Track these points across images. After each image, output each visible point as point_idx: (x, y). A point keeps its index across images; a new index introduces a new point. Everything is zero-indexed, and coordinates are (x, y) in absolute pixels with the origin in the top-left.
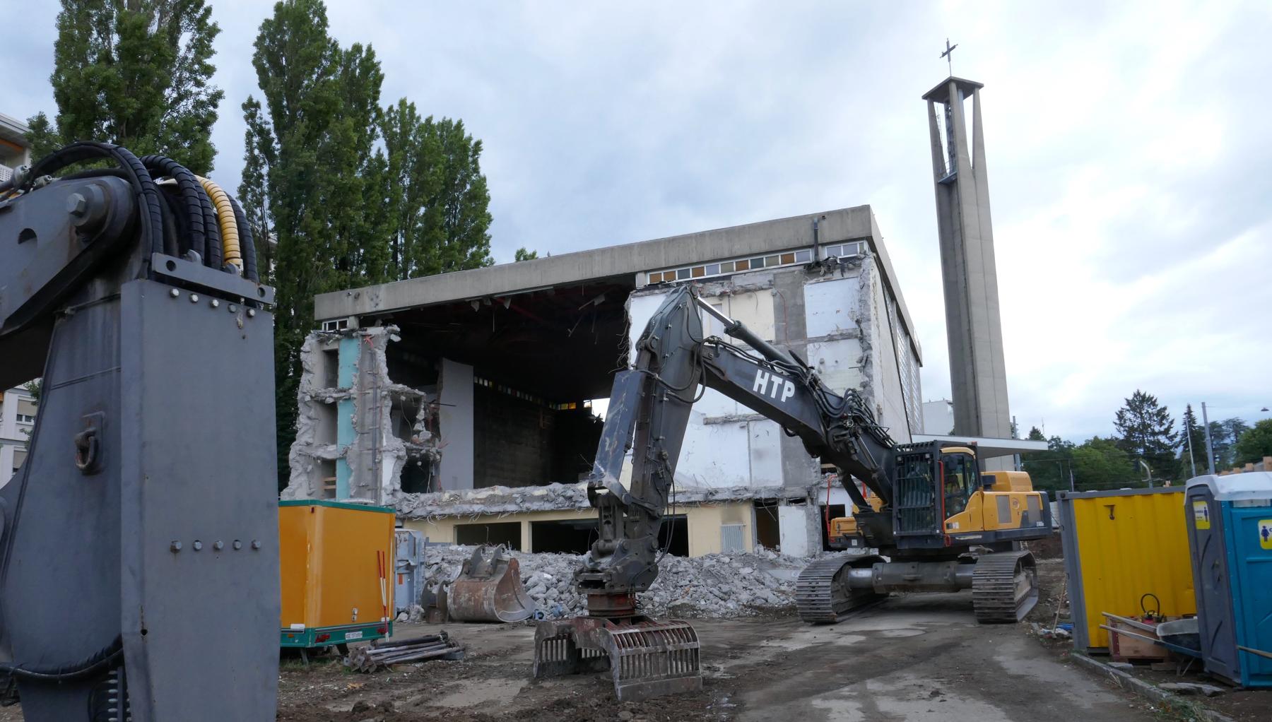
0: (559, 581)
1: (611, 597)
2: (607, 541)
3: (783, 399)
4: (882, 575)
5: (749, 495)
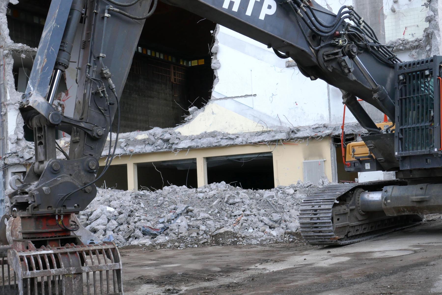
0: (120, 213)
1: (39, 218)
3: (262, 17)
4: (391, 198)
5: (328, 132)
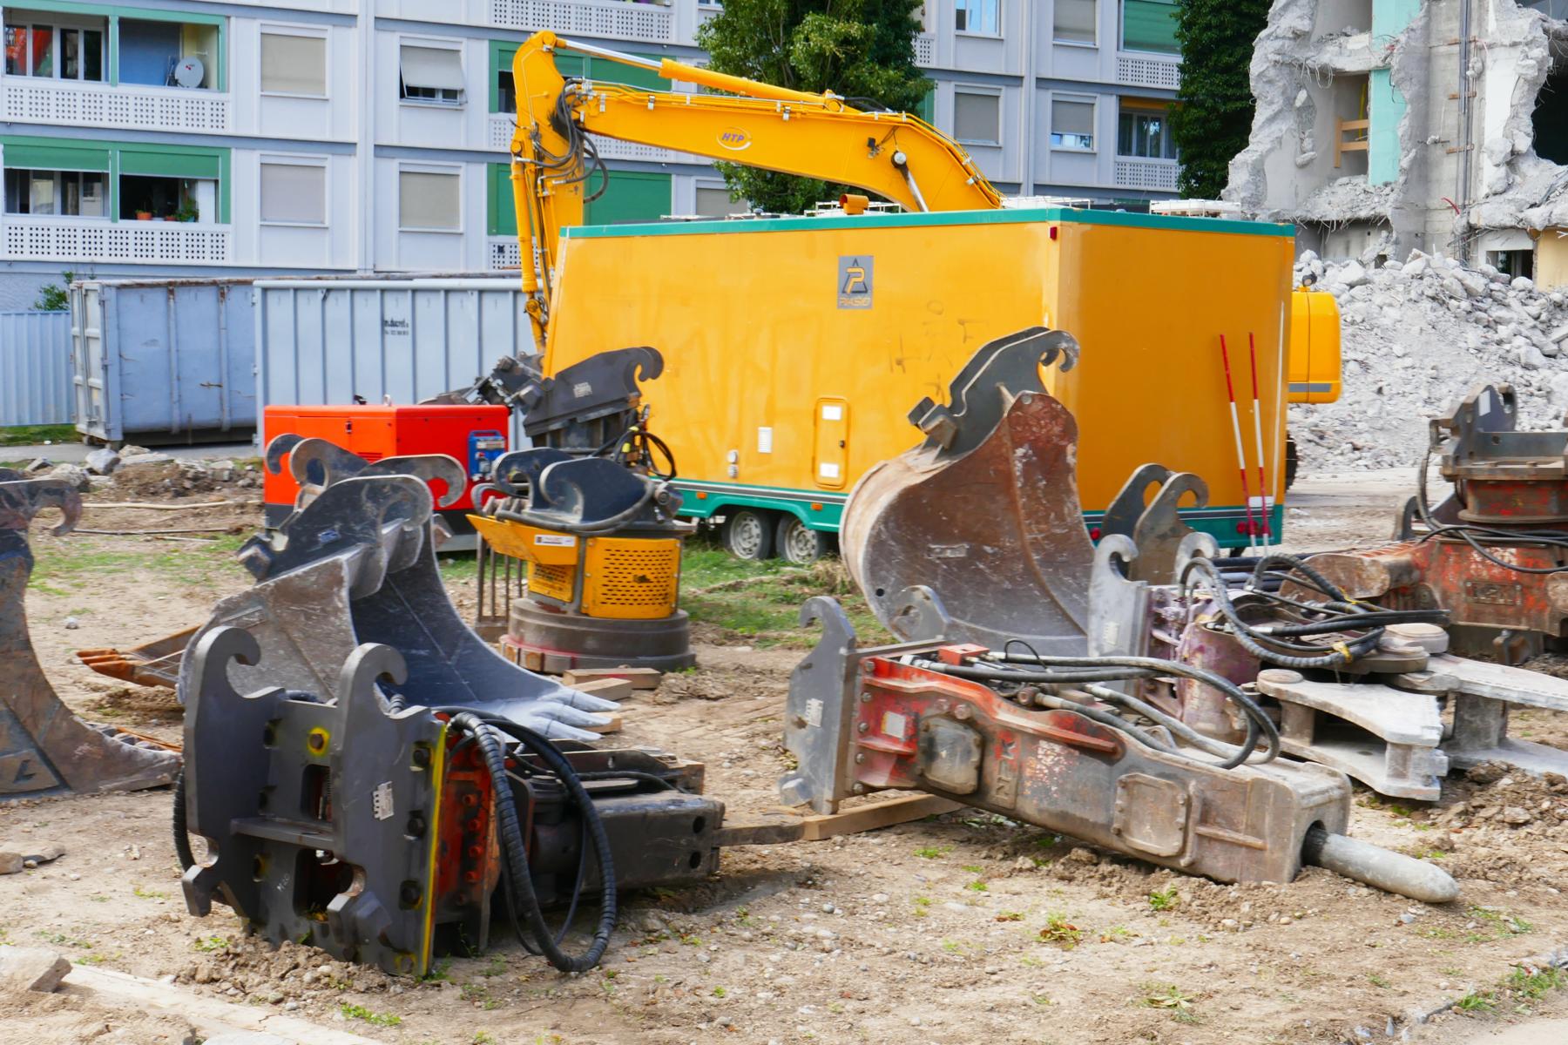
2: (1180, 739)
